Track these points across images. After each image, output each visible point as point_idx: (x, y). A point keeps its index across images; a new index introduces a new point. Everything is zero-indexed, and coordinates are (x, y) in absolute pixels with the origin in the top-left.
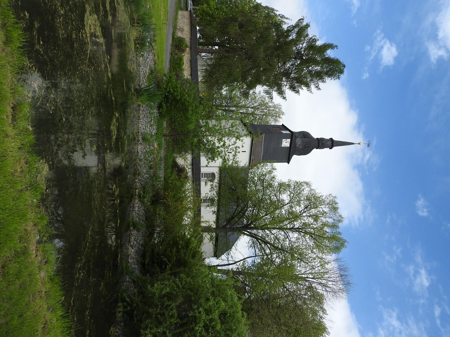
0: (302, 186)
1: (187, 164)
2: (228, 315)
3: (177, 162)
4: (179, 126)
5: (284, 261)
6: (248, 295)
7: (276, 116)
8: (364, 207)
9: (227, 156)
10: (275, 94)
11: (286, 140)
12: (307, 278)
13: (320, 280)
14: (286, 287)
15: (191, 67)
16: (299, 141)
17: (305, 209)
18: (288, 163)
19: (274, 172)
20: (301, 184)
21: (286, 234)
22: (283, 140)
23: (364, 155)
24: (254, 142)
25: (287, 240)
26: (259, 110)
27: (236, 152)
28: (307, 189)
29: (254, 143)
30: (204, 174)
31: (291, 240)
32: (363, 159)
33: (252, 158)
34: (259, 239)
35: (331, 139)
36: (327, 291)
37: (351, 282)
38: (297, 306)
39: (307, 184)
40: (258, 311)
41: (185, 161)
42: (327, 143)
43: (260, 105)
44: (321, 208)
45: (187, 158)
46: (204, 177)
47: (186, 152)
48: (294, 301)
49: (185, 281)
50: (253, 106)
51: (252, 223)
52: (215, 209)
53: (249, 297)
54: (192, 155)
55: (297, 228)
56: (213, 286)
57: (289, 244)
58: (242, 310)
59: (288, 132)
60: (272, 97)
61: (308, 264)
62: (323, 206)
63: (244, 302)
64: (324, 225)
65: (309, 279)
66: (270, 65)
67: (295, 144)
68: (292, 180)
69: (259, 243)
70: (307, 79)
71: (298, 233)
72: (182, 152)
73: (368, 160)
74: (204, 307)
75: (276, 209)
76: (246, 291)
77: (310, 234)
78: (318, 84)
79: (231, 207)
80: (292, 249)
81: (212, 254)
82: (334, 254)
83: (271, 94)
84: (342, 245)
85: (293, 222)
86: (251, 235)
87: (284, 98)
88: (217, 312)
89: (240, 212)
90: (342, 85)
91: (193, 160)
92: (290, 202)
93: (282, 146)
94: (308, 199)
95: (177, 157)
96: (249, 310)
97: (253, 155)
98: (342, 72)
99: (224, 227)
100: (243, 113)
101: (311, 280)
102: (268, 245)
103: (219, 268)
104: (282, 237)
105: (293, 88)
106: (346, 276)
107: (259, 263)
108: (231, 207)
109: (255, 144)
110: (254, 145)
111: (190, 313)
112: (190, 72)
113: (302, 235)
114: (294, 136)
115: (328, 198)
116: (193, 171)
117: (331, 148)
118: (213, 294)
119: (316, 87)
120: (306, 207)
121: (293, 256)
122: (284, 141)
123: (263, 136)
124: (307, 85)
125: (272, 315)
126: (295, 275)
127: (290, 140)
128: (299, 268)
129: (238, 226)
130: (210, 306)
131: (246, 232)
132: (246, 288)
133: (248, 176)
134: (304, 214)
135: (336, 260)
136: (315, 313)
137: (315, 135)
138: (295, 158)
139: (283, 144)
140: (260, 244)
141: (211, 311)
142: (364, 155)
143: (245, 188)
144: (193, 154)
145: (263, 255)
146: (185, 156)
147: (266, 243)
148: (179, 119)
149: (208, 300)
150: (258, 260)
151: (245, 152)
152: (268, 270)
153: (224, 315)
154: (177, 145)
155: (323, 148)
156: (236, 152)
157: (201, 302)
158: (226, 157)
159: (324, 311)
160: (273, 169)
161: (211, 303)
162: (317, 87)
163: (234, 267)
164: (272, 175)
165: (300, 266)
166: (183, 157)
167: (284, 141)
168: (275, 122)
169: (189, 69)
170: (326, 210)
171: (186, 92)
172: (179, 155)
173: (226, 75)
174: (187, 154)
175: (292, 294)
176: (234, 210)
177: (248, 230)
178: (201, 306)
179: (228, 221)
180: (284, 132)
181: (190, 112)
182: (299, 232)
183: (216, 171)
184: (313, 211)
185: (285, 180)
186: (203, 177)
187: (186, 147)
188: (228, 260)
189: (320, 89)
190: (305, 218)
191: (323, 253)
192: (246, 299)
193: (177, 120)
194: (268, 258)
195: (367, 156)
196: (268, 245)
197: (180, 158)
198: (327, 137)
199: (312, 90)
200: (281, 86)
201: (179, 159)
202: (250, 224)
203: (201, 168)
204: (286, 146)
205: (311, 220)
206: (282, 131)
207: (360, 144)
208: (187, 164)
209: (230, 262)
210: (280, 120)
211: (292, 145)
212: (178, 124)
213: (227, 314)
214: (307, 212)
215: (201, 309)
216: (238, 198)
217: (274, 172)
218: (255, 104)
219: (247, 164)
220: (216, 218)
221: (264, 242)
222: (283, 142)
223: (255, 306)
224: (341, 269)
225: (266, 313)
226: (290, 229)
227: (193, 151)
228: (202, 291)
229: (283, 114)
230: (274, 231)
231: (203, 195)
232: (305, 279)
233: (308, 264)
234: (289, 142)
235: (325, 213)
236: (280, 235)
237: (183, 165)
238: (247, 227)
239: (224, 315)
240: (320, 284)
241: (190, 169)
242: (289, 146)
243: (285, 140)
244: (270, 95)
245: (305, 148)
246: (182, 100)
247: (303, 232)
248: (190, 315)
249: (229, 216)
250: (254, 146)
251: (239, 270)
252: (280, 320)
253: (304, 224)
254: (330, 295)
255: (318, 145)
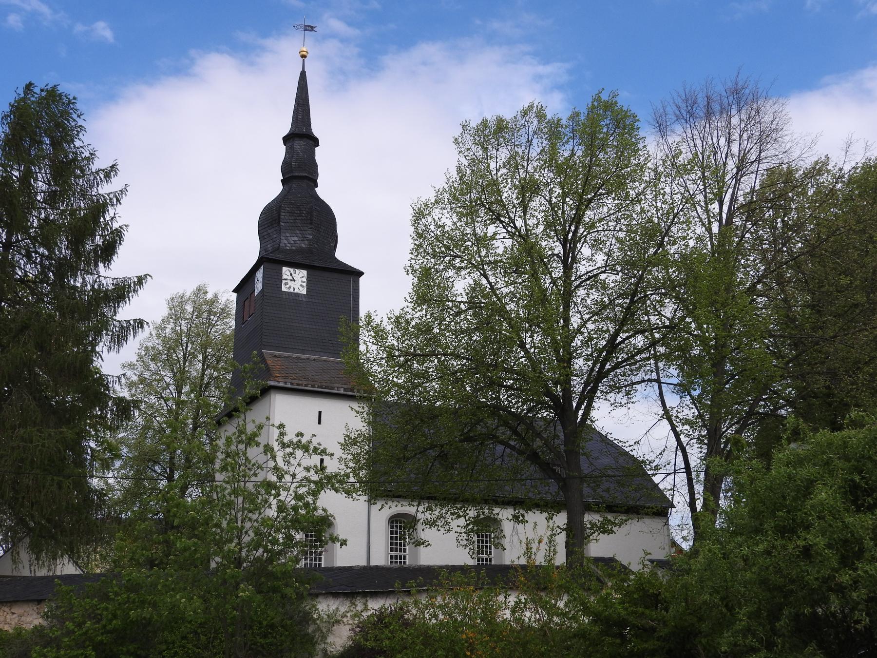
0: (427, 230)
1: (349, 615)
2: (857, 478)
3: (342, 649)
4: (214, 647)
5: (670, 288)
6: (785, 406)
7: (210, 312)
8: (492, 39)
9: (309, 474)
10: (126, 312)
11: (284, 282)
12: (720, 221)
13: (727, 178)
14: (754, 285)
15: (10, 602)
16: (290, 241)
17: (501, 222)
18: (361, 274)
19: (377, 320)
20: (420, 235)
21: (582, 282)
22: (284, 289)
23: (333, 36)
24: (289, 385)
25: (603, 276)
26: (187, 369)
27: (298, 445)
28: (436, 213)
29: (292, 384)
30: (394, 553)
31: (599, 265)
32: (344, 40)
33: (342, 391)
34: (603, 366)
35: (286, 140)
36: (759, 160)
37: (730, 84)
38: (811, 250)
39: (419, 215)
40: (833, 374)
41: (338, 622)
42: (298, 154)
43: (170, 363)
44: (497, 170)
45: (328, 616)
46: (405, 551)
47: (307, 618)
48: (795, 261)
49: (745, 636)
50: (172, 388)
51: (549, 393)
52: (505, 514)
53: (790, 403)
54: (320, 599)
55: (564, 246)
56: (758, 531)
57: (613, 270)
58: (836, 427)
59: (259, 274)
60: (135, 321)
61: (678, 213)
62: (493, 166)
63: (806, 420)
64: (551, 160)
65: (724, 216)
66: (24, 328)
67: (300, 251)
68: (408, 264)
69: (613, 368)
70: (80, 209)
71: (579, 245)
72: (308, 634)
73: (350, 24)
74: (834, 570)
75: (502, 311)
76: (773, 414)
77: (582, 205)
78: (97, 172)
79: (500, 460)
80: (628, 265)
81: (651, 524)
82: (642, 134)
83: (125, 324)
84: (609, 106)
85: (546, 260)
86: (589, 396)
87: (140, 281)
88: (849, 520)
89: (515, 432)
90: (111, 97)
91: (335, 595)
92: (479, 267)
93: (304, 292)
94: (470, 213)
95: (325, 651)
96: (830, 405)
97: (332, 388)
98: (53, 95)
99: (564, 484)
100: (195, 419)
101: (725, 208)
102: (619, 339)
103: (699, 505)
104: (595, 295)
105: (108, 252)
106: (709, 99)
107: (680, 368)
108: (498, 463)
109: (297, 382)
110: (298, 385)
111: (858, 622)
112: (30, 604)
113: (585, 233)
114: (272, 256)
115: (469, 149)
116: (374, 595)
117: (315, 142)
118: (786, 531)
119: (109, 177)
120: (497, 218)
121: (654, 261)
122: (290, 288)
123: (268, 354)
124: (99, 208)
125: (844, 330)
126: (713, 255)
127: (285, 269)
128: (692, 243)
129: (562, 435)
130: (829, 546)
131: (581, 412)
132: (762, 413)
133: (394, 403)
134: (519, 223)
135: (662, 130)
136: (827, 196)
137: (273, 188)
138: (344, 254)
139: (297, 291)
140: (618, 366)
141: (846, 541)
142: (333, 36)
143: (433, 415)
144: (317, 596)
145: (657, 358)
146: (322, 621)
147: (612, 346)
148: (190, 646)
149: (807, 552)
150: (672, 374)
151: (320, 413)
152: (704, 341)
153: (859, 493)
154: (281, 651)
155: (316, 165)
156: (298, 445)
157: (817, 579)
158: (312, 479)
159: (818, 169)
160: (369, 324)
161: (821, 541)
162: (108, 175)
163: (696, 454)
164: (389, 328)
165: (684, 238)
166: (324, 630)
167: (290, 288)
168: (228, 315)
169: (18, 610)
170: (503, 154)
171: (76, 626)
172: (316, 643)
173: (53, 480)
174: (315, 616)
175: (774, 270)
176: (508, 450)
177: (574, 405)
178: (831, 578)
179: (547, 468)
180: (259, 287)
181: (147, 612)
182: (575, 240)
183: (383, 512)
184: (509, 194)
185: (407, 284)
186: (402, 554)
187: (291, 618)
188: (675, 473)
189: (112, 167)
190: (531, 222)
191: (641, 167)
192: (798, 413)
193: (194, 652)
194: (663, 341)
195: (337, 25)
196: (619, 339)
197: (329, 640)
198: (281, 151)
199: (118, 189)
200: (99, 291)
201: (331, 644)
202: (554, 398)
203: (374, 563)
204: (305, 279)
205: (536, 202)
206: (256, 294)
207: (304, 53)
208: (349, 615)
209: (681, 464)
210: (222, 300)
211: (301, 261)
212: (206, 648)
213: (852, 480)
214: (512, 216)
215: (845, 578)
216: (468, 439)
217: (377, 320)
218: (168, 380)
219: (355, 405)
220: (538, 513)
221: (609, 353)
222: (291, 290)
223: (819, 384)
224: (692, 115)
225: (836, 350)
226: (568, 268)
227: (301, 597)
228: (778, 571)
229: (201, 291)
230: (575, 321)
231: (463, 557)
232: (727, 225)
233: (678, 213)
234: (292, 270)
235: (513, 157)
236: (589, 302)
237: (353, 629)
238: (563, 409)
239: (859, 493)
240: (737, 179)
241: (366, 605)
242: (305, 272)
243: (286, 284)
244: (128, 328)
245: (311, 220)
246: (101, 642)
247: (577, 228)
248: (867, 620)
249: (531, 469)
250: (301, 385)
251: (704, 436)
252: (856, 306)
253: (549, 225)
254: (771, 151)
255: (305, 181)
